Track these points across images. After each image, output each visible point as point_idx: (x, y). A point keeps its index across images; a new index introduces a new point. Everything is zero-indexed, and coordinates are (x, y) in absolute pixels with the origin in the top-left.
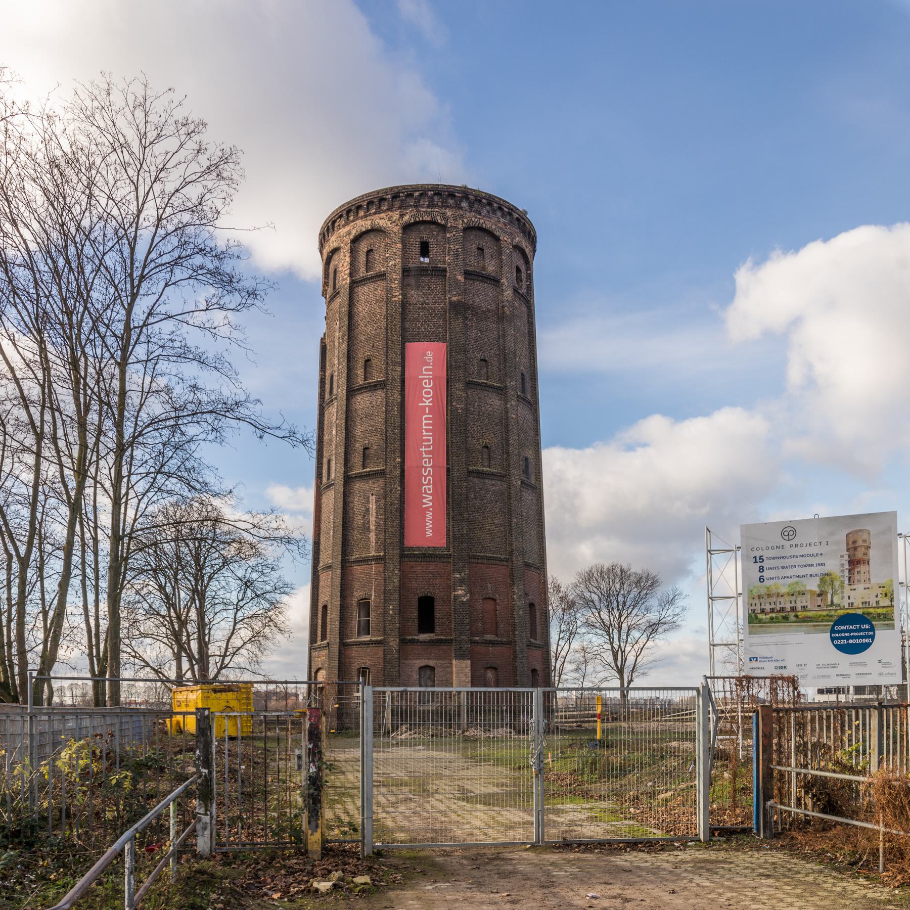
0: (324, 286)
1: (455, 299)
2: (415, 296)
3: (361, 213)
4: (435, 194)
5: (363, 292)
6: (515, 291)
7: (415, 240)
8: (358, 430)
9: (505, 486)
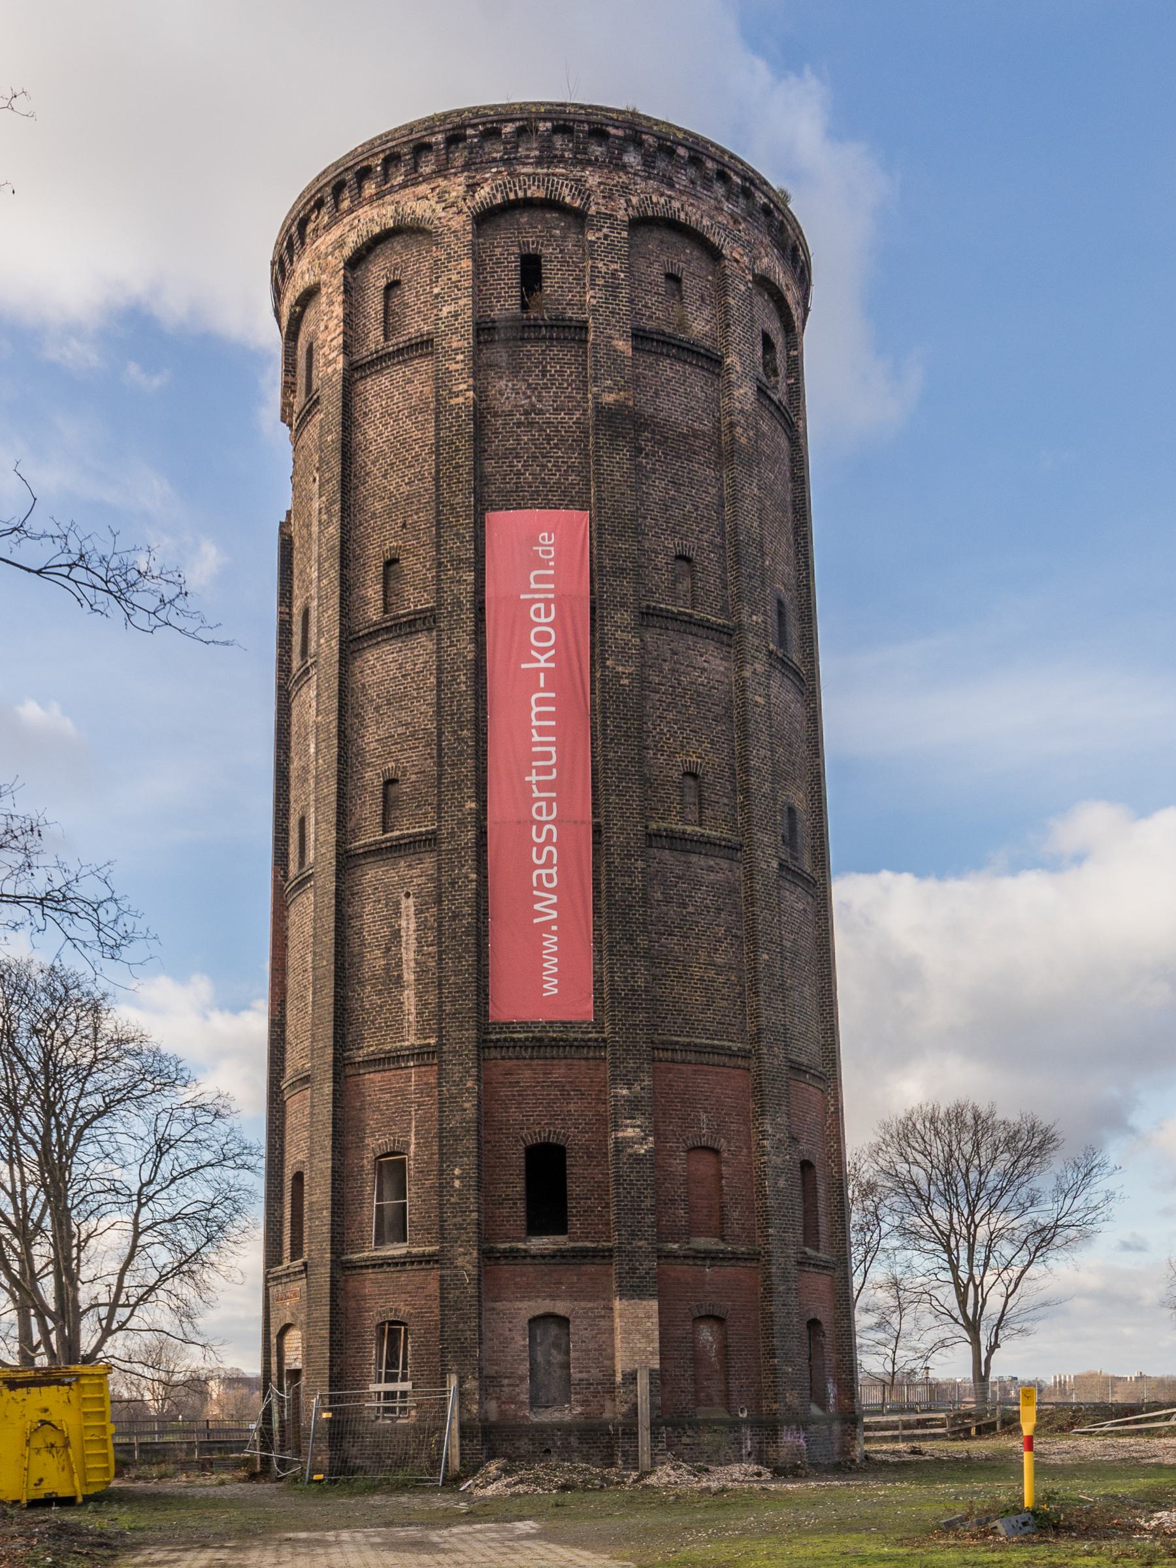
0: (284, 395)
1: (609, 398)
2: (507, 392)
3: (370, 189)
4: (556, 130)
5: (383, 392)
6: (761, 391)
7: (505, 250)
8: (371, 737)
9: (740, 873)
